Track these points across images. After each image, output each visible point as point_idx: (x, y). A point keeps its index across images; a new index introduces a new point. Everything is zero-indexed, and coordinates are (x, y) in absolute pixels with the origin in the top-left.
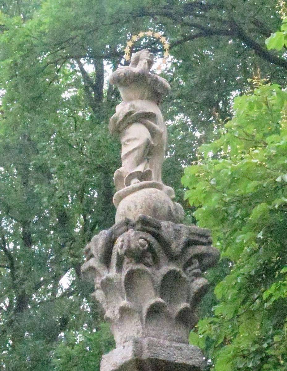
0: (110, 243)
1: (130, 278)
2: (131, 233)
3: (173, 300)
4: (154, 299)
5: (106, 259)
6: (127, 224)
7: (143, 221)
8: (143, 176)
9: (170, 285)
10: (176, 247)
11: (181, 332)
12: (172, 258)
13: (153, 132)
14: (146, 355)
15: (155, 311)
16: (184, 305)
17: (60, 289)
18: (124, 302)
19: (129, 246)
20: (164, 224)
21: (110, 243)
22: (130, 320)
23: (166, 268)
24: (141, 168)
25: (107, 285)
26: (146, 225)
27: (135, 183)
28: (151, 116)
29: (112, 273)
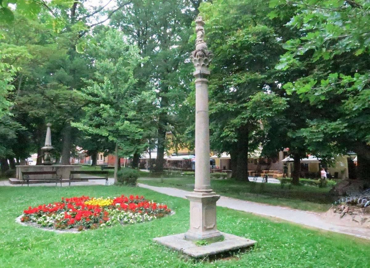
0: (196, 53)
1: (199, 60)
2: (200, 52)
3: (206, 63)
4: (203, 63)
5: (195, 56)
6: (199, 50)
7: (202, 50)
8: (201, 41)
9: (206, 61)
10: (207, 54)
11: (206, 69)
12: (206, 56)
13: (203, 32)
14: (202, 73)
15: (203, 65)
16: (208, 64)
17: (208, 16)
18: (198, 64)
19: (229, 182)
20: (205, 50)
21: (196, 53)
22: (205, 111)
23: (205, 58)
24: (200, 39)
25: (195, 60)
26: (202, 51)
27: (200, 42)
28: (202, 29)
29: (196, 58)
